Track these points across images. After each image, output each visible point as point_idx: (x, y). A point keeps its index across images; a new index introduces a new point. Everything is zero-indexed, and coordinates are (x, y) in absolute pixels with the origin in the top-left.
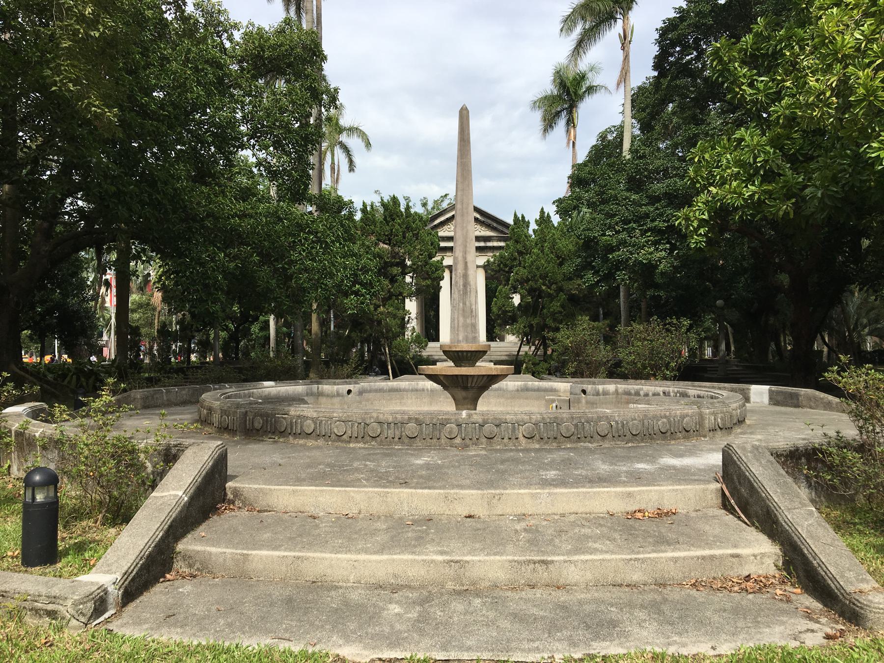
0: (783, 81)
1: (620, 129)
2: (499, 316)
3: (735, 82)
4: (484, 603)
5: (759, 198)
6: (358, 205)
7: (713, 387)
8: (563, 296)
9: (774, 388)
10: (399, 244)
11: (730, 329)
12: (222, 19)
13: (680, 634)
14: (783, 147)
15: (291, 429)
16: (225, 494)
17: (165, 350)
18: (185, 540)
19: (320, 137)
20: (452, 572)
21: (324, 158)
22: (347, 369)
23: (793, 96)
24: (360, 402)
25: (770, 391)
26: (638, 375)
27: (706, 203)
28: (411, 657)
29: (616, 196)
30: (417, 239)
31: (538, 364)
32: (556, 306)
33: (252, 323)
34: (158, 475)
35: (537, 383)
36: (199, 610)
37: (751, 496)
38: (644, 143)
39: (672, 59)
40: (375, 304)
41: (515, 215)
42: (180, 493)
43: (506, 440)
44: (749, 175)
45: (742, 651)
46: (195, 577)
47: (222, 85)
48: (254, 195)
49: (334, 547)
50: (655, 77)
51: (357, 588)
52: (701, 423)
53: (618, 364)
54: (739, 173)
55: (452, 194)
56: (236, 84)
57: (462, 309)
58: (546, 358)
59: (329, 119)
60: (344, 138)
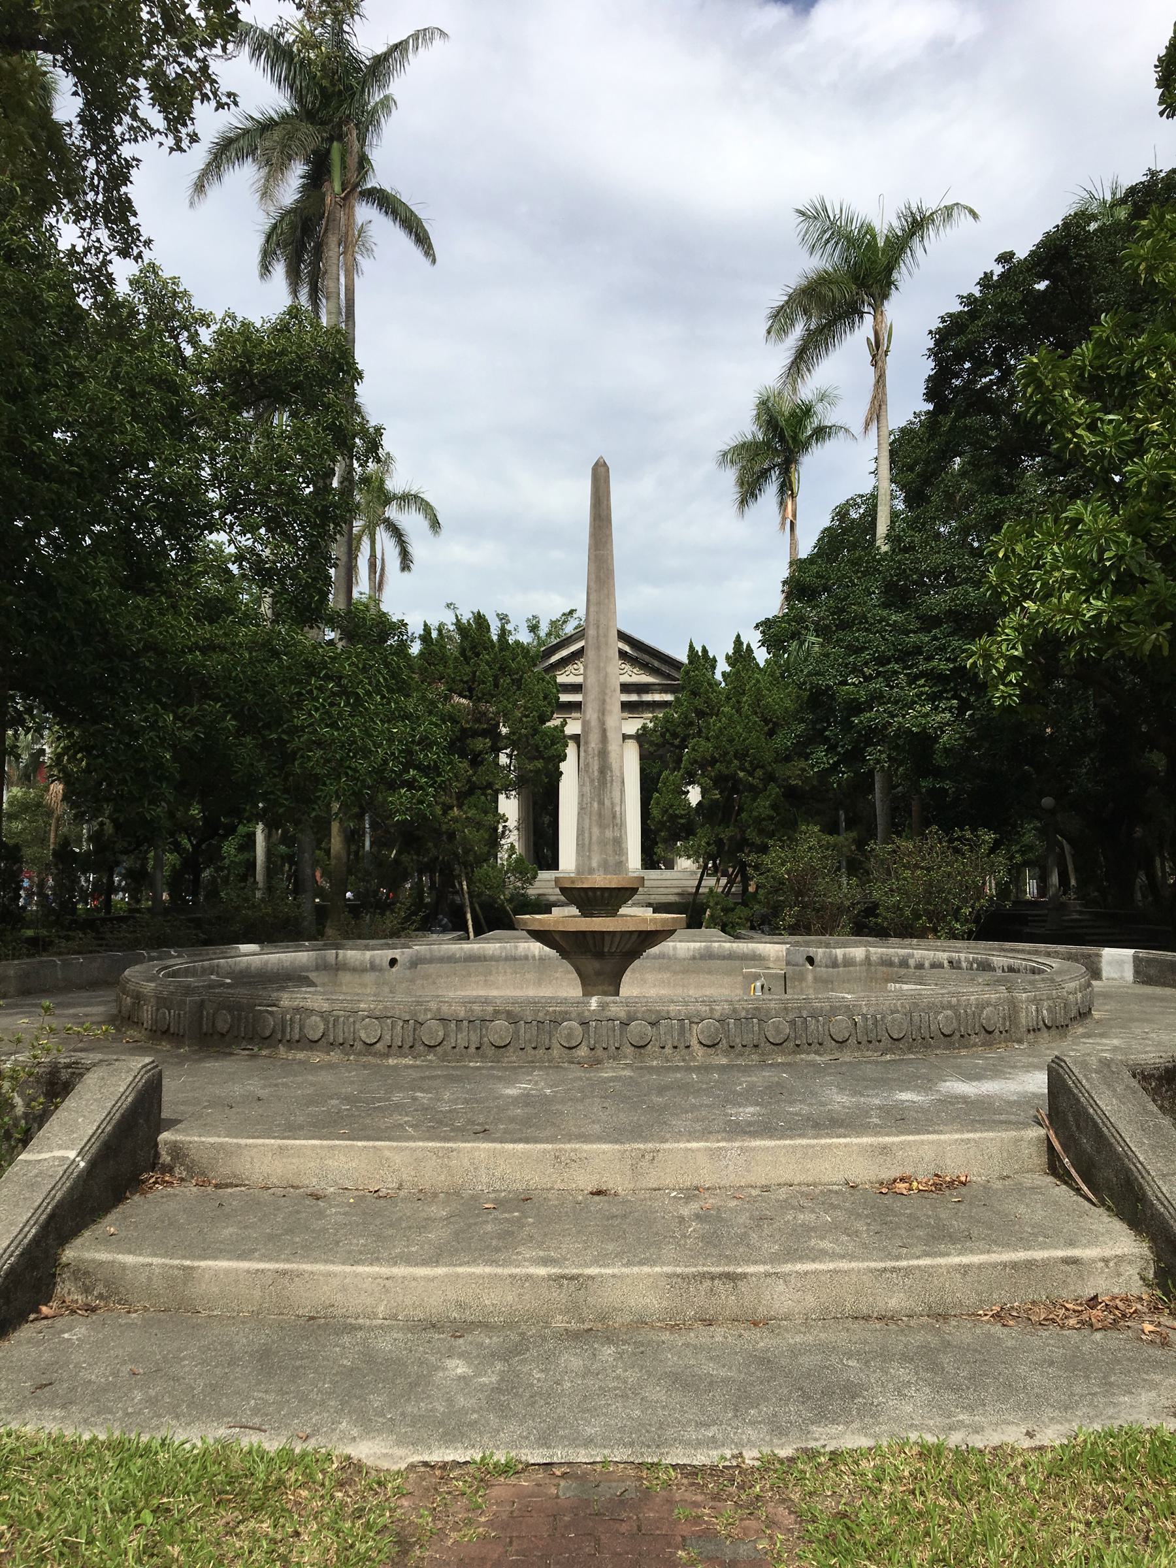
0: (1148, 421)
1: (872, 501)
2: (662, 823)
3: (1064, 422)
4: (621, 1354)
5: (1109, 622)
6: (415, 628)
7: (1036, 953)
8: (774, 790)
9: (1143, 953)
10: (488, 697)
11: (1067, 847)
12: (180, 307)
13: (970, 1409)
14: (1148, 534)
15: (283, 1032)
16: (157, 1155)
17: (67, 884)
18: (78, 1242)
19: (350, 511)
20: (563, 1297)
21: (358, 548)
22: (391, 921)
23: (1165, 447)
24: (412, 981)
25: (1136, 959)
26: (907, 930)
27: (1019, 629)
28: (483, 1459)
29: (865, 617)
30: (519, 688)
31: (733, 910)
32: (762, 806)
33: (225, 837)
34: (34, 1119)
35: (727, 945)
36: (97, 1375)
37: (1099, 1152)
38: (912, 524)
39: (957, 382)
40: (444, 804)
41: (691, 647)
42: (72, 1154)
43: (668, 1050)
44: (1092, 580)
45: (1081, 1438)
46: (94, 1310)
47: (175, 423)
48: (231, 612)
49: (349, 1252)
50: (928, 413)
51: (391, 1327)
52: (1012, 1015)
53: (871, 910)
54: (1073, 577)
55: (581, 613)
56: (202, 418)
57: (601, 808)
58: (746, 899)
59: (366, 480)
60: (392, 512)
